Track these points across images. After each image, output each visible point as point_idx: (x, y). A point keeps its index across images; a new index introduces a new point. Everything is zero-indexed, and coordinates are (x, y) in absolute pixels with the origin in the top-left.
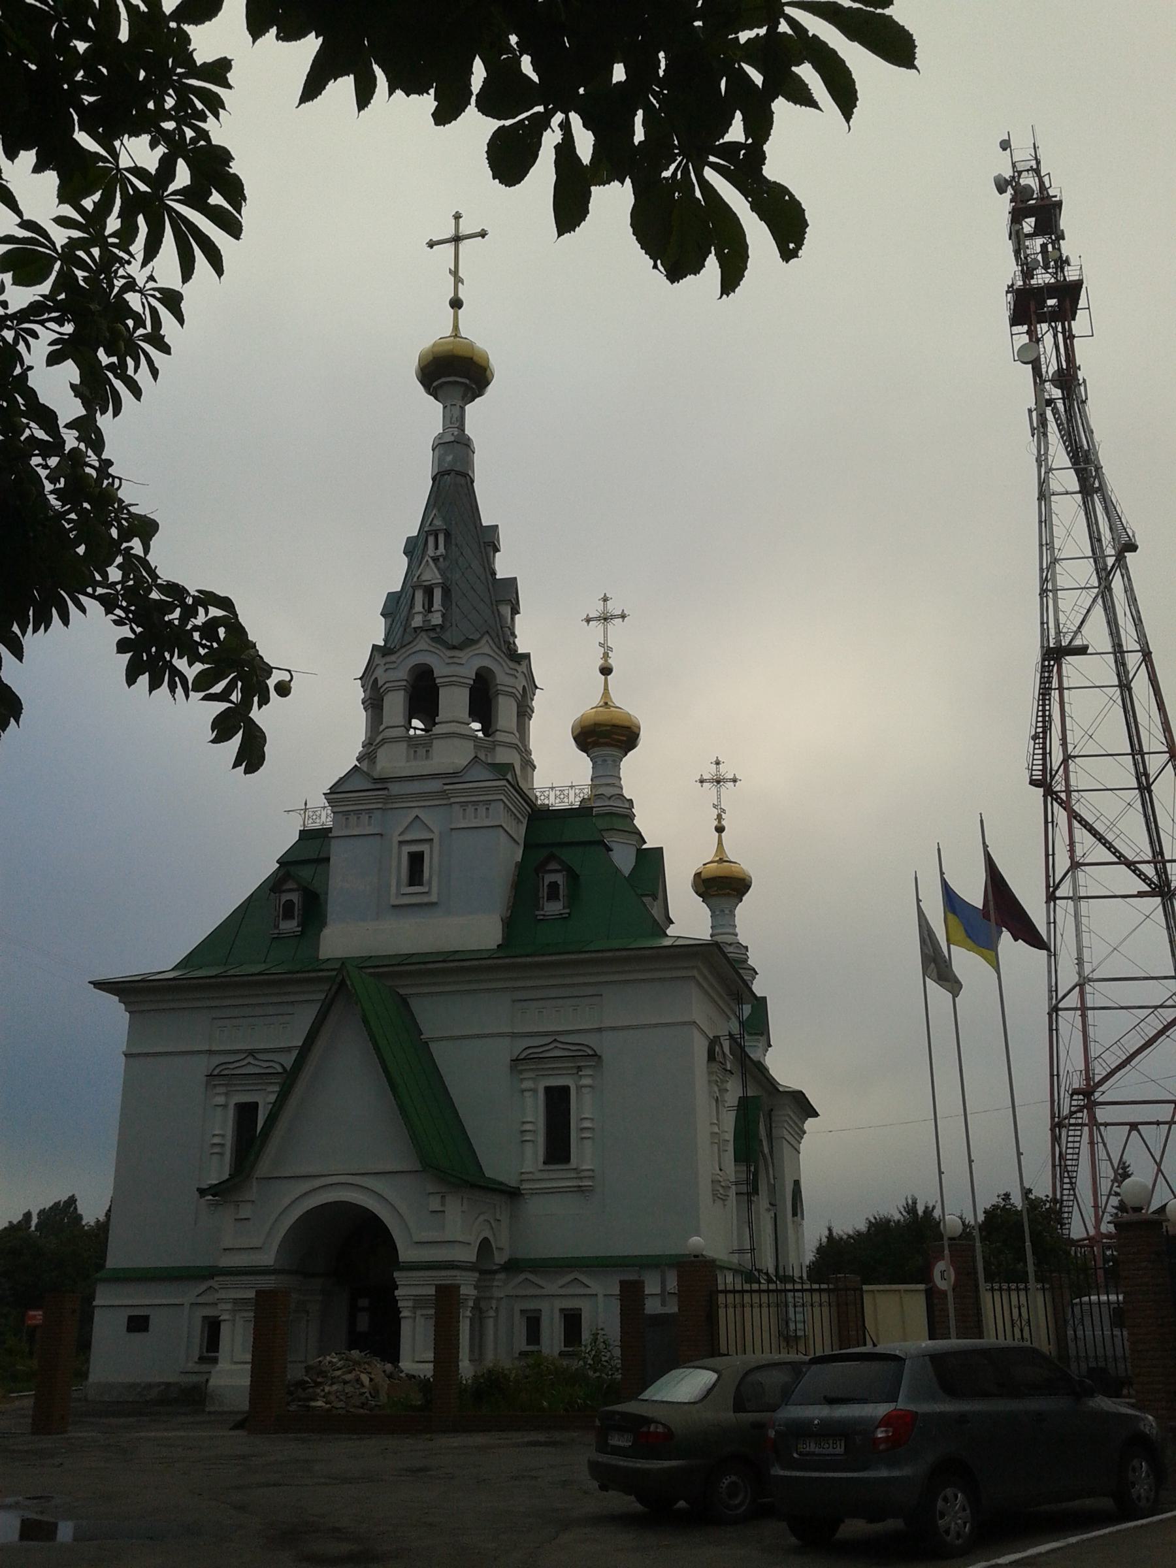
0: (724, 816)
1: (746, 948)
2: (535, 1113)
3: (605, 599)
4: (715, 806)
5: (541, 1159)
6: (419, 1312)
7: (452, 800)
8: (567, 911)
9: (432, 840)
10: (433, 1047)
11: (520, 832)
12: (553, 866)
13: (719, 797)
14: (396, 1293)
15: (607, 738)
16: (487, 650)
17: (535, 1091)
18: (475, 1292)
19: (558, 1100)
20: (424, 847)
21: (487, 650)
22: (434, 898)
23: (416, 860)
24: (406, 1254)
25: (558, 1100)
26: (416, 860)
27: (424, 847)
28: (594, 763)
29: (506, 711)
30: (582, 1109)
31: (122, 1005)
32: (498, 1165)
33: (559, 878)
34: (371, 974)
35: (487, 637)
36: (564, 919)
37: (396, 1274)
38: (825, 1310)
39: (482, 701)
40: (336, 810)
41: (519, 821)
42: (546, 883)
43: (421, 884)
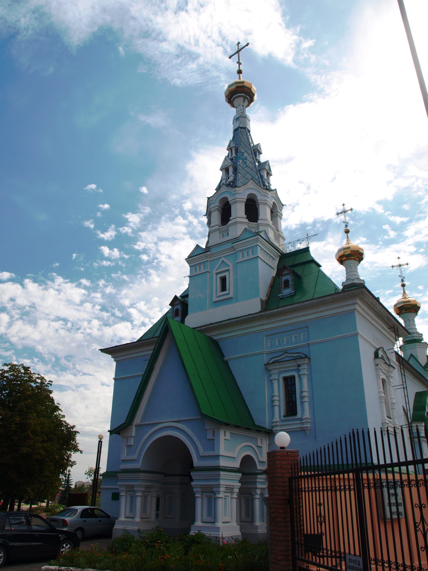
0: (404, 280)
1: (422, 334)
2: (279, 391)
3: (344, 205)
4: (400, 276)
5: (283, 414)
6: (204, 494)
7: (237, 250)
8: (294, 292)
9: (229, 270)
10: (229, 362)
11: (275, 264)
12: (286, 272)
13: (401, 272)
14: (192, 483)
15: (350, 257)
16: (252, 186)
17: (278, 380)
18: (240, 484)
19: (290, 384)
20: (226, 274)
21: (252, 186)
22: (231, 295)
23: (223, 280)
24: (196, 462)
25: (290, 384)
26: (223, 280)
27: (226, 274)
28: (346, 268)
29: (265, 213)
30: (303, 386)
31: (113, 359)
32: (263, 419)
33: (289, 277)
34: (199, 331)
35: (251, 181)
36: (292, 296)
37: (192, 473)
38: (352, 492)
39: (252, 209)
40: (192, 265)
41: (273, 259)
42: (283, 280)
43: (225, 290)
